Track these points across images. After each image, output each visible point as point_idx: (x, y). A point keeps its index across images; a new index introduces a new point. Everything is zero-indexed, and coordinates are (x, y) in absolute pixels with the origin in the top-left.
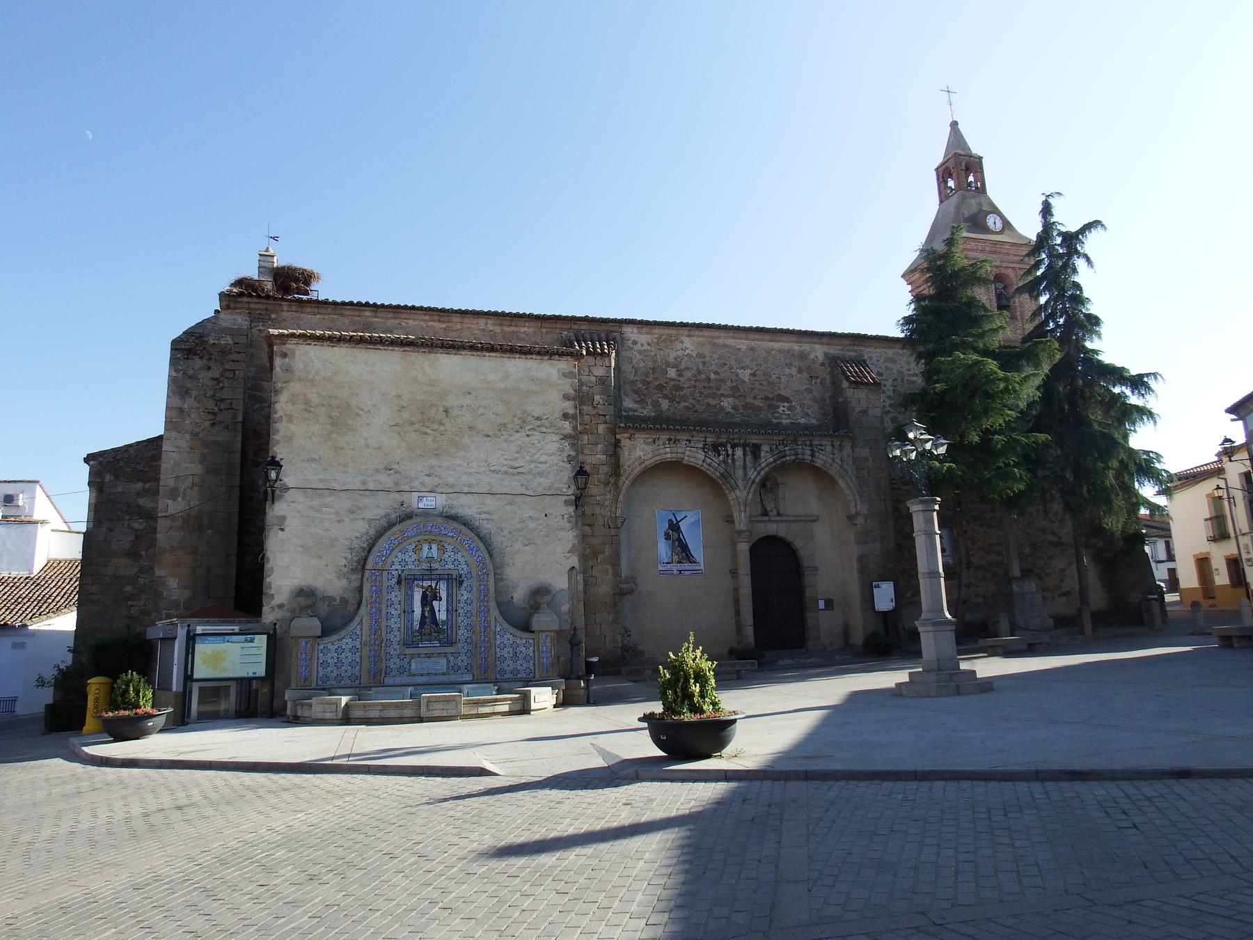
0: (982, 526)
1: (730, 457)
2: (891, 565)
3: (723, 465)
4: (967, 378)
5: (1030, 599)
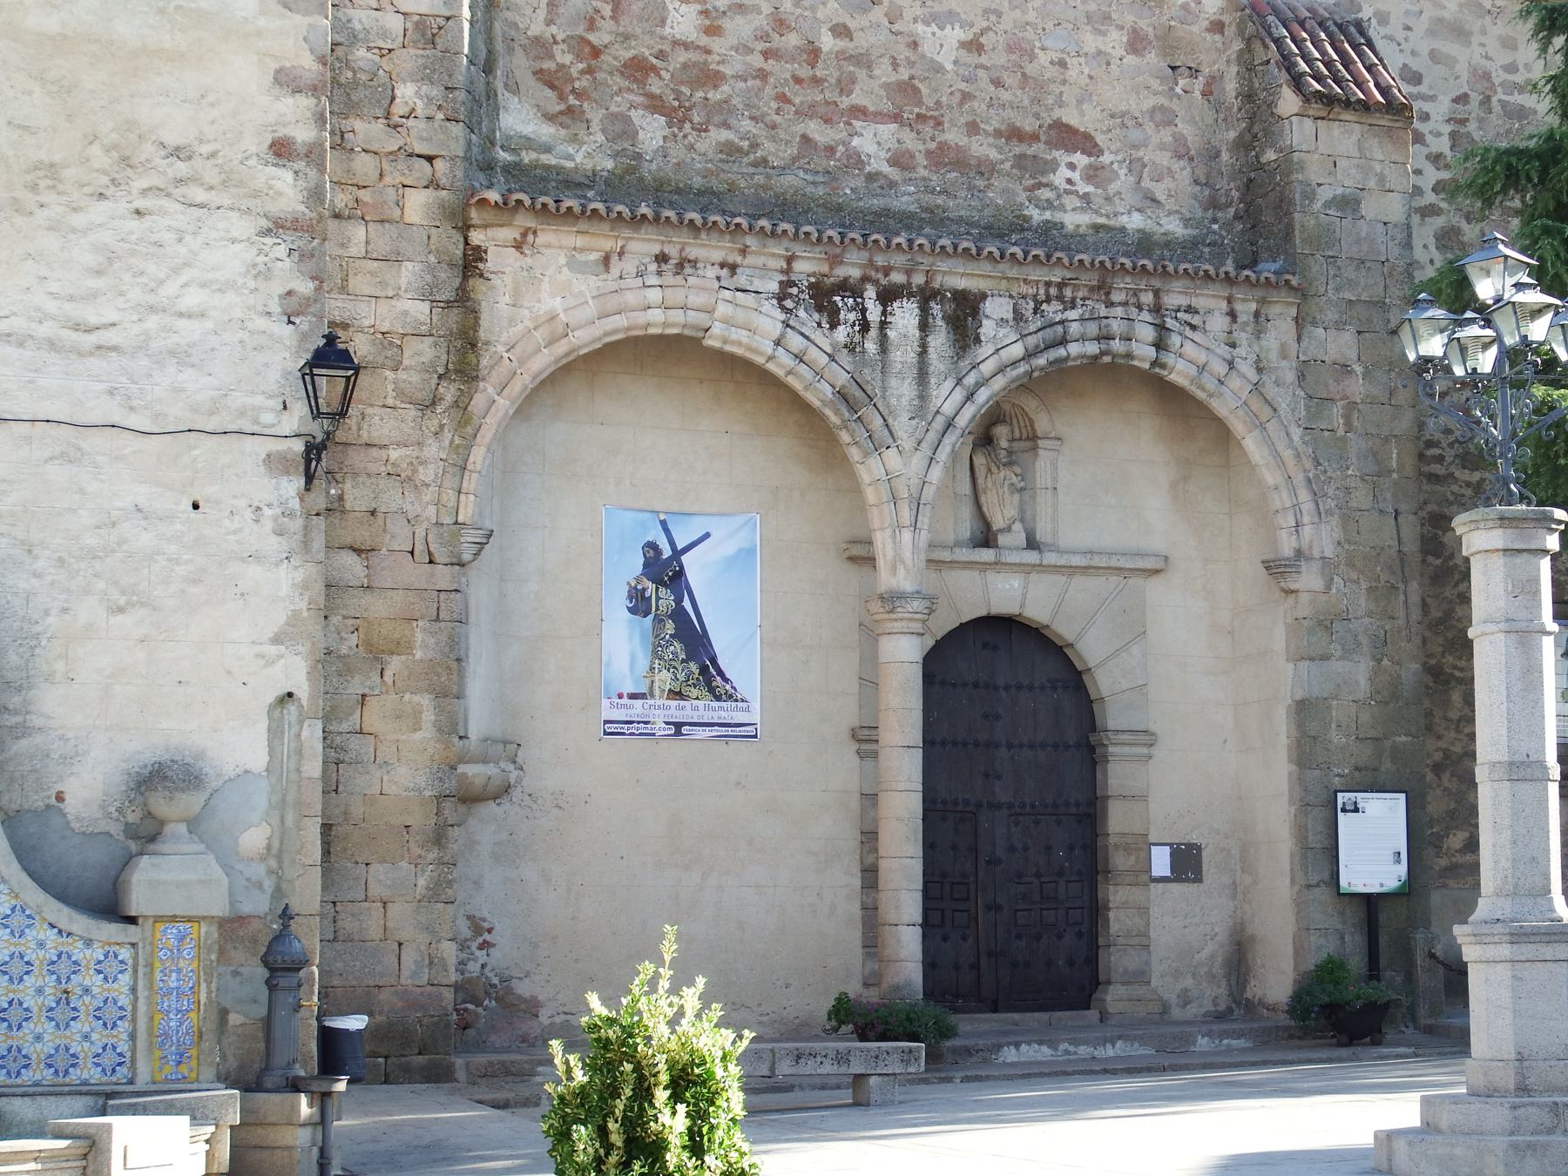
2: (1404, 739)
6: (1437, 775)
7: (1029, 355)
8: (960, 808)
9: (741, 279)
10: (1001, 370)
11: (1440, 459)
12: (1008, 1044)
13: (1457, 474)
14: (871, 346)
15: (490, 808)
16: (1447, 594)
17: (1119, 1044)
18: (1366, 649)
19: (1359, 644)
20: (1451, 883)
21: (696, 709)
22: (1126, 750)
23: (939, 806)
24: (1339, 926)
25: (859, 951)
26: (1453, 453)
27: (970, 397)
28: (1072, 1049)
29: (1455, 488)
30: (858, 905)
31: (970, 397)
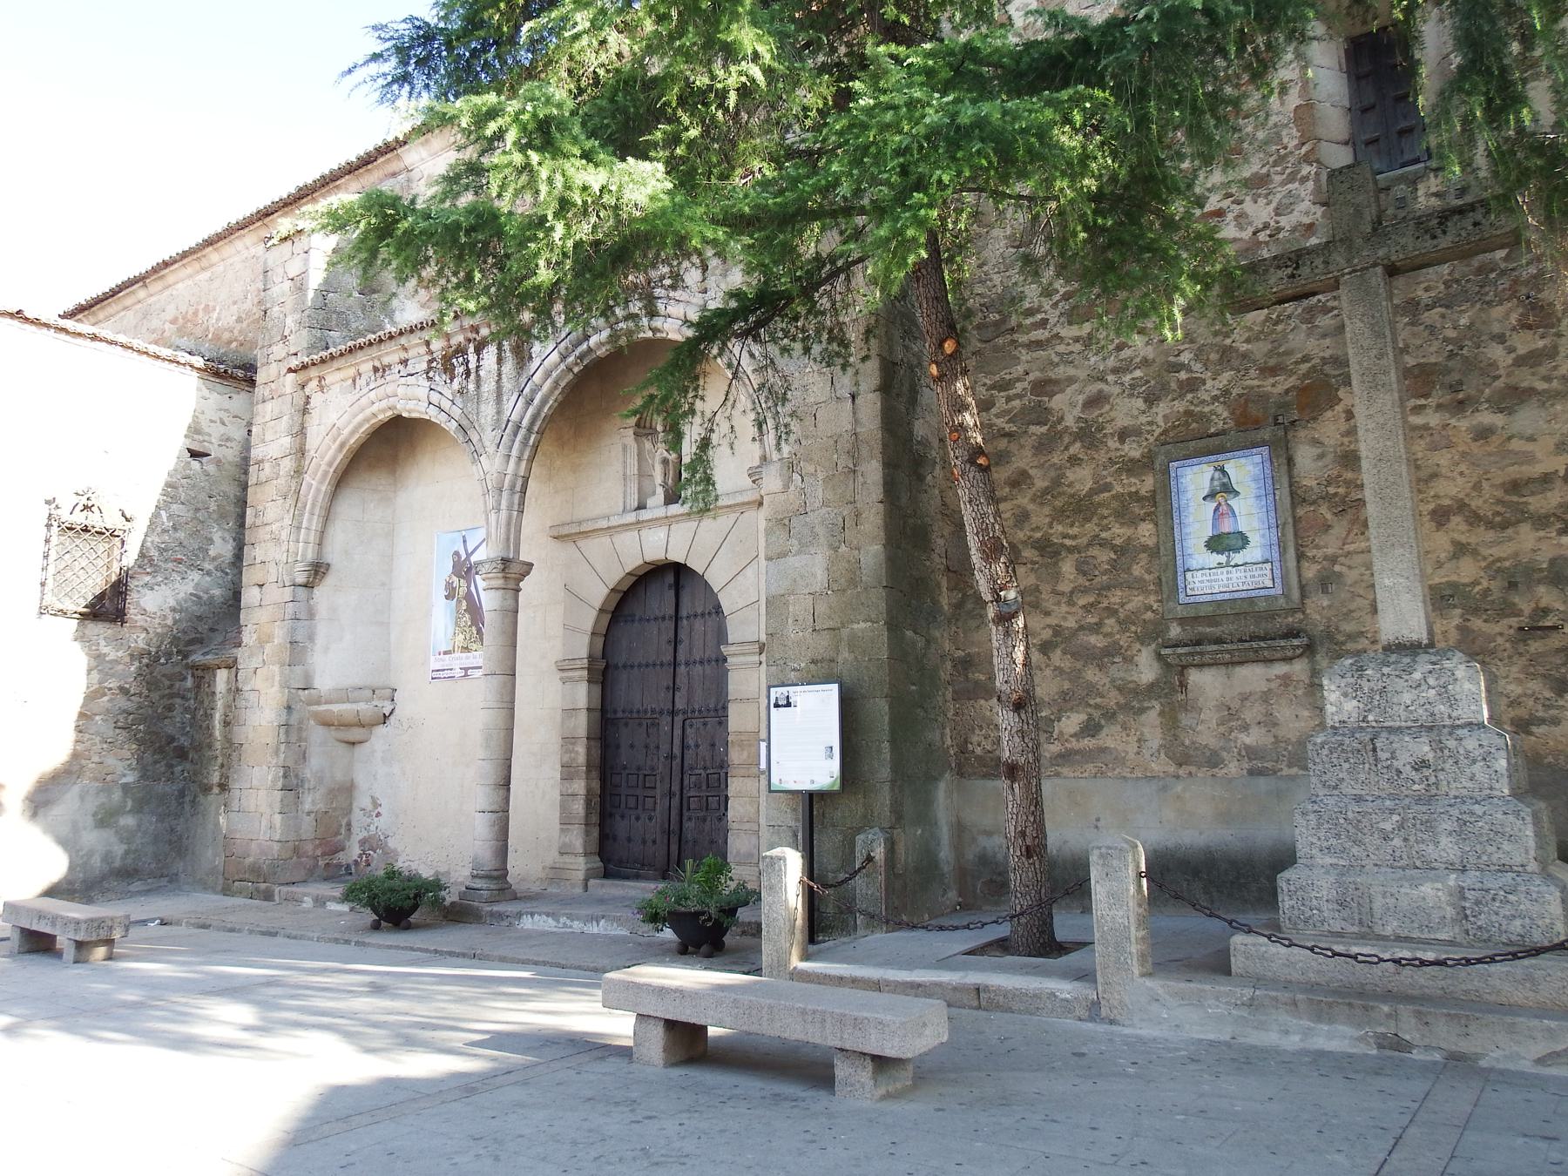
0: (1460, 406)
1: (473, 376)
2: (862, 625)
3: (458, 401)
4: (1502, 23)
5: (1421, 765)
6: (1045, 654)
7: (563, 358)
8: (649, 715)
9: (410, 369)
10: (548, 374)
11: (1043, 323)
12: (527, 913)
13: (1063, 333)
14: (471, 387)
15: (380, 730)
16: (1055, 460)
17: (602, 922)
18: (822, 540)
19: (815, 536)
20: (1065, 771)
21: (475, 657)
22: (742, 659)
23: (635, 715)
24: (792, 824)
25: (558, 826)
26: (1058, 313)
27: (529, 402)
28: (568, 922)
29: (1061, 348)
30: (558, 792)
31: (529, 402)
